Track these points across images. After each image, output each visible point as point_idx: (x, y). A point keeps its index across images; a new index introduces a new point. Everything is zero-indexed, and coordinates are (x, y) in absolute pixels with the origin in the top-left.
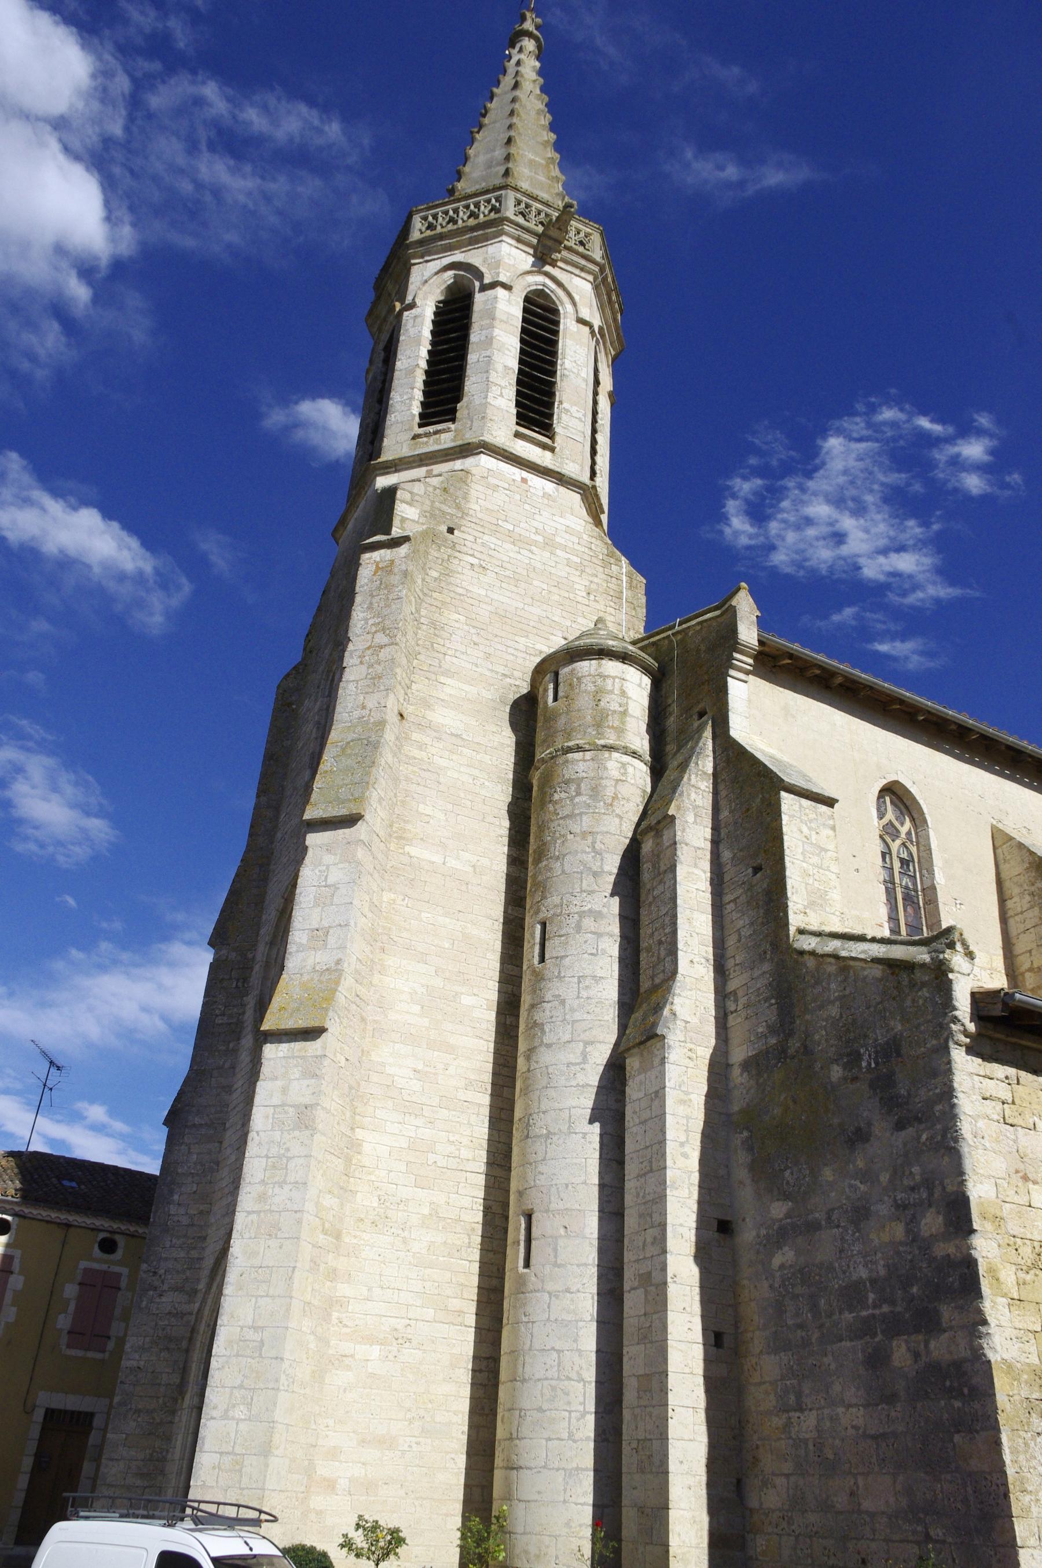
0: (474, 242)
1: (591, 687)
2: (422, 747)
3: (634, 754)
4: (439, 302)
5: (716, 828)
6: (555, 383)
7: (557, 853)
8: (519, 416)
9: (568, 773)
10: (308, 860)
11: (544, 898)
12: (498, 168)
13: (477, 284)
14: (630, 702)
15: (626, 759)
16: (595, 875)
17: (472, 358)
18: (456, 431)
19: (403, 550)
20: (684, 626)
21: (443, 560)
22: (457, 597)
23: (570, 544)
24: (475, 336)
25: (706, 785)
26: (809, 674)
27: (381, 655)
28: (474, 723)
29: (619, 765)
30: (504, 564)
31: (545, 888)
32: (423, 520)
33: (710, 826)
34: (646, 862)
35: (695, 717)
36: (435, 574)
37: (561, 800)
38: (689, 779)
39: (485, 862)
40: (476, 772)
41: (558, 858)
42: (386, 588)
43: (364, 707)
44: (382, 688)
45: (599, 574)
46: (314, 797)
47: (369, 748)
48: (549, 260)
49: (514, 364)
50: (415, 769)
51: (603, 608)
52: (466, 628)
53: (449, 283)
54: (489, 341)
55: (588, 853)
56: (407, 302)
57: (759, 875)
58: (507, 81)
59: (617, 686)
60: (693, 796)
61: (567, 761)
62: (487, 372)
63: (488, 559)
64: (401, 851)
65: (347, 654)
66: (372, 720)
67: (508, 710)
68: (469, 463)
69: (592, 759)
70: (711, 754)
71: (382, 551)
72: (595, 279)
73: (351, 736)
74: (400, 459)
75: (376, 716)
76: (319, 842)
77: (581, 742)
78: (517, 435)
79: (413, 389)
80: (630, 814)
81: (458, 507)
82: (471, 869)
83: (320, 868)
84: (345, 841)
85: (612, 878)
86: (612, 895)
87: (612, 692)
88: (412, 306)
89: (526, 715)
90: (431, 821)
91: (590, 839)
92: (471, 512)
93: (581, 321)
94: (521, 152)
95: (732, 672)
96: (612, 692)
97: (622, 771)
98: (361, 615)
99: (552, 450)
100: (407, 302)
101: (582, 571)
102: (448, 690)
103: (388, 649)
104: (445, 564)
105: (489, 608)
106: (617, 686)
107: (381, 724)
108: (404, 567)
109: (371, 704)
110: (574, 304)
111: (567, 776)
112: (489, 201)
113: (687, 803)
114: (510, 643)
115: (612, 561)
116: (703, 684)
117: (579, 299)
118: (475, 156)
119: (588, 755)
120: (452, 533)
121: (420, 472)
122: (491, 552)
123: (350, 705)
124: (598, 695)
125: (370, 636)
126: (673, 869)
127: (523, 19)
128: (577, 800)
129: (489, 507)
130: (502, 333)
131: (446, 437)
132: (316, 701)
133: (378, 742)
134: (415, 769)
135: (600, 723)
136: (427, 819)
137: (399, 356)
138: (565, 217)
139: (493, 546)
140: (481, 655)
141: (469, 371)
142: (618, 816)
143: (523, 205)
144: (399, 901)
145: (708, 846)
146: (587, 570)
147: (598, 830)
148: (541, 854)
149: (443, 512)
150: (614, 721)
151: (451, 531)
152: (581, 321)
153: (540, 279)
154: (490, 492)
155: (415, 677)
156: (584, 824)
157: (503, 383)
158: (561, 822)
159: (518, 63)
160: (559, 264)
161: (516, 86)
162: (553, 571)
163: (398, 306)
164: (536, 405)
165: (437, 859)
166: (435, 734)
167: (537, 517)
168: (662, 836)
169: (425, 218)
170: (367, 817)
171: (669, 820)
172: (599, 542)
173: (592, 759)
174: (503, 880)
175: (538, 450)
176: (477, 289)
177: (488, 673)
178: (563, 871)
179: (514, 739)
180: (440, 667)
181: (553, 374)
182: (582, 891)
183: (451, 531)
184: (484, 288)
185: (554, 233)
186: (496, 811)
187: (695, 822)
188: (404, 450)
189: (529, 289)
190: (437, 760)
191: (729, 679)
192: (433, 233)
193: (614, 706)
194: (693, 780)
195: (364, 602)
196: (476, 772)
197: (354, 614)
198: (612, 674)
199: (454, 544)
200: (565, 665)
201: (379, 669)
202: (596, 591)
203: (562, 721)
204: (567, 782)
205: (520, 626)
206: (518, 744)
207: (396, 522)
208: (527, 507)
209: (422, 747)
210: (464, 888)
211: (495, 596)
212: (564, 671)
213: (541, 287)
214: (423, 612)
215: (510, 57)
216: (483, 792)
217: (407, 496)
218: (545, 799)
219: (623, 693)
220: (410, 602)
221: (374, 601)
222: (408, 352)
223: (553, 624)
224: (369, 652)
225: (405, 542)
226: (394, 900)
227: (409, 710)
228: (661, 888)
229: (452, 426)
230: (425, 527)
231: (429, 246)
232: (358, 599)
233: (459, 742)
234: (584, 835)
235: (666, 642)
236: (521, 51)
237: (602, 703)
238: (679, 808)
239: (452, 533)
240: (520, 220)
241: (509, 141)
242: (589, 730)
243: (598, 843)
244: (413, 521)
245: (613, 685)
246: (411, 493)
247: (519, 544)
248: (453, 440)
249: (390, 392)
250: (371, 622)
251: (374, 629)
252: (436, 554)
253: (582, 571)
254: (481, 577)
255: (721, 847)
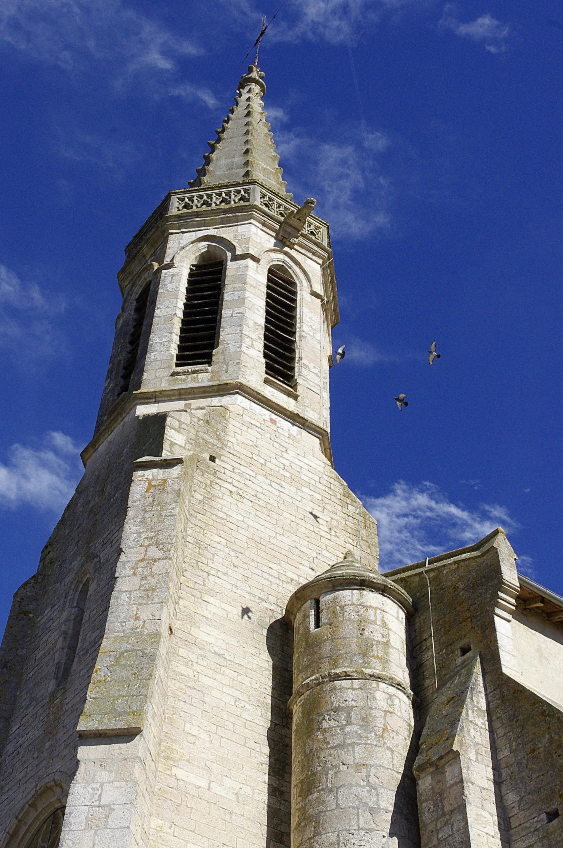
0: (226, 222)
1: (354, 616)
2: (188, 663)
3: (399, 686)
4: (193, 266)
5: (496, 768)
6: (294, 342)
7: (330, 785)
8: (268, 366)
9: (337, 700)
10: (79, 775)
11: (317, 834)
12: (238, 170)
13: (229, 254)
14: (391, 633)
15: (392, 690)
16: (372, 811)
17: (226, 313)
18: (212, 372)
19: (176, 471)
20: (436, 565)
21: (206, 485)
22: (218, 520)
23: (313, 482)
24: (228, 296)
25: (482, 721)
26: (556, 619)
27: (154, 568)
28: (235, 644)
29: (387, 696)
30: (258, 494)
31: (317, 822)
32: (188, 446)
33: (491, 765)
34: (426, 800)
35: (458, 653)
36: (200, 497)
37: (331, 728)
38: (467, 715)
39: (248, 790)
40: (237, 694)
41: (331, 791)
42: (159, 504)
43: (137, 618)
44: (156, 600)
45: (338, 512)
46: (88, 706)
47: (145, 660)
48: (288, 243)
49: (262, 321)
50: (182, 685)
51: (342, 543)
52: (227, 550)
53: (203, 251)
54: (242, 301)
55: (364, 787)
56: (165, 263)
57: (555, 822)
58: (240, 110)
59: (379, 617)
60: (472, 732)
61: (335, 688)
62: (241, 325)
63: (244, 488)
64: (168, 772)
65: (119, 564)
66: (146, 632)
67: (265, 634)
68: (226, 400)
69: (360, 688)
70: (483, 690)
71: (155, 470)
72: (323, 263)
73: (124, 646)
74: (161, 392)
75: (149, 628)
76: (92, 757)
77: (349, 669)
78: (266, 381)
79: (171, 333)
80: (400, 748)
81: (219, 438)
82: (234, 797)
83: (94, 786)
84: (121, 757)
85: (389, 816)
86: (391, 835)
87: (374, 622)
88: (170, 266)
89: (282, 637)
90: (197, 742)
91: (364, 771)
92: (229, 444)
93: (315, 294)
94: (256, 161)
95: (497, 611)
96: (374, 622)
97: (390, 702)
98: (134, 528)
99: (296, 397)
100: (165, 263)
101: (324, 508)
102: (211, 608)
103: (161, 563)
104: (208, 489)
105: (246, 533)
106: (379, 617)
107: (157, 635)
108: (176, 487)
109: (145, 615)
110: (309, 280)
111: (336, 704)
112: (239, 192)
113: (468, 740)
114: (266, 569)
115: (349, 501)
116: (465, 620)
117: (311, 275)
118: (217, 159)
119: (357, 684)
120: (214, 461)
121: (181, 404)
122: (247, 482)
123: (123, 615)
124: (362, 624)
125: (143, 549)
126: (462, 809)
127: (251, 70)
128: (348, 729)
129: (245, 441)
130: (252, 296)
131: (203, 377)
132: (63, 610)
133: (154, 654)
134: (182, 685)
135: (365, 652)
136: (192, 739)
137: (158, 305)
138: (305, 211)
139: (248, 477)
140: (240, 577)
141: (224, 323)
142: (389, 748)
143: (266, 199)
144: (166, 829)
145: (492, 786)
146: (328, 507)
147: (371, 762)
148: (310, 785)
149: (206, 442)
150: (377, 651)
151: (212, 459)
152: (315, 294)
153: (281, 256)
154: (245, 428)
155: (183, 594)
156: (356, 755)
157: (254, 336)
158: (332, 751)
159: (248, 99)
160: (296, 247)
161: (249, 114)
162: (300, 505)
163: (156, 266)
164: (280, 358)
165: (203, 784)
166: (200, 652)
167: (285, 455)
168: (443, 773)
169: (183, 200)
170: (144, 732)
171: (451, 756)
172: (336, 483)
173: (360, 688)
174: (265, 812)
175: (285, 397)
176: (229, 258)
177: (246, 595)
178: (338, 805)
179: (271, 663)
180: (204, 585)
181: (293, 334)
182: (359, 829)
183: (212, 459)
184: (235, 258)
185: (294, 222)
186: (257, 736)
187: (477, 761)
188: (163, 385)
189: (272, 264)
190: (202, 678)
191: (496, 618)
192: (190, 211)
193: (377, 637)
194: (471, 717)
195: (136, 516)
196: (237, 694)
197: (126, 526)
198: (373, 605)
199: (216, 471)
200: (326, 593)
201: (153, 581)
202: (336, 527)
203: (327, 648)
204: (336, 710)
205: (273, 553)
206: (275, 668)
207: (166, 446)
208: (276, 445)
209: (188, 663)
210: (228, 818)
211: (251, 523)
212: (325, 599)
213: (281, 263)
214: (189, 532)
215: (240, 95)
216: (245, 715)
217: (176, 424)
218: (311, 724)
219: (384, 625)
220: (181, 519)
221: (147, 515)
222: (166, 303)
223: (302, 555)
224: (142, 564)
225: (178, 464)
226: (161, 827)
227: (177, 625)
228: (447, 831)
229: (209, 368)
230: (192, 452)
231: (185, 221)
232: (131, 513)
233: (221, 661)
234: (358, 767)
235: (417, 579)
236: (250, 91)
237: (366, 633)
238: (461, 744)
239: (214, 461)
240: (264, 208)
241: (247, 152)
242: (355, 658)
243: (372, 776)
244: (181, 446)
245: (375, 616)
246: (179, 421)
247: (270, 477)
248: (210, 380)
249: (149, 334)
250: (143, 536)
251: (147, 543)
252: (200, 478)
253: (324, 508)
254: (239, 504)
255: (504, 788)
